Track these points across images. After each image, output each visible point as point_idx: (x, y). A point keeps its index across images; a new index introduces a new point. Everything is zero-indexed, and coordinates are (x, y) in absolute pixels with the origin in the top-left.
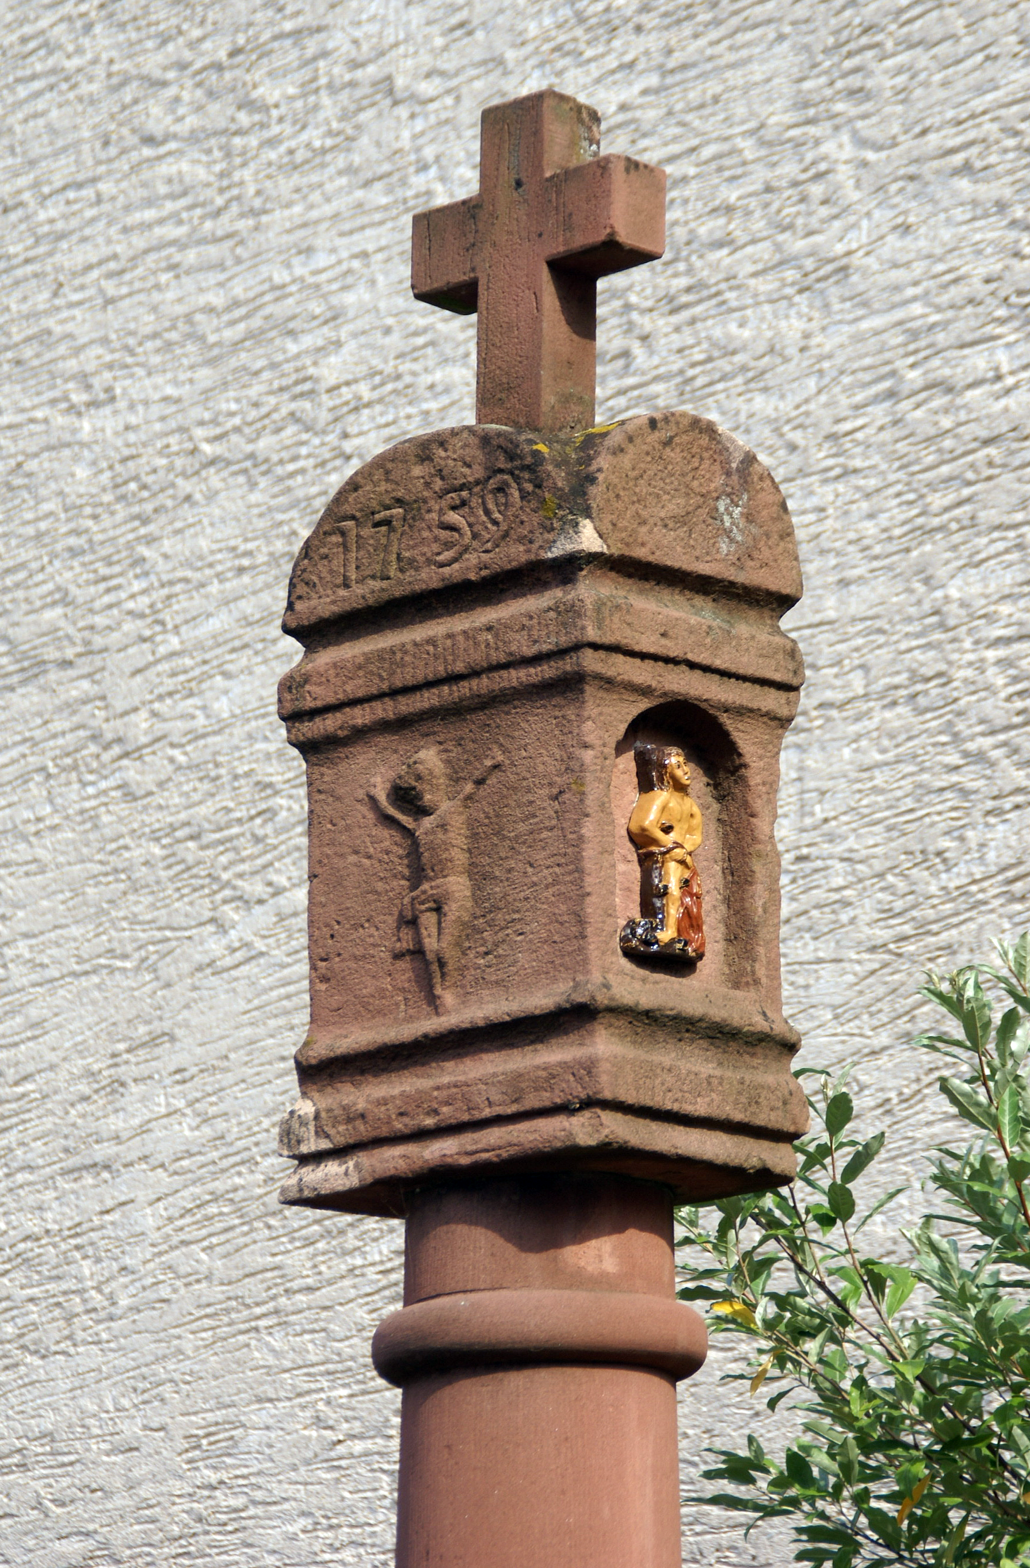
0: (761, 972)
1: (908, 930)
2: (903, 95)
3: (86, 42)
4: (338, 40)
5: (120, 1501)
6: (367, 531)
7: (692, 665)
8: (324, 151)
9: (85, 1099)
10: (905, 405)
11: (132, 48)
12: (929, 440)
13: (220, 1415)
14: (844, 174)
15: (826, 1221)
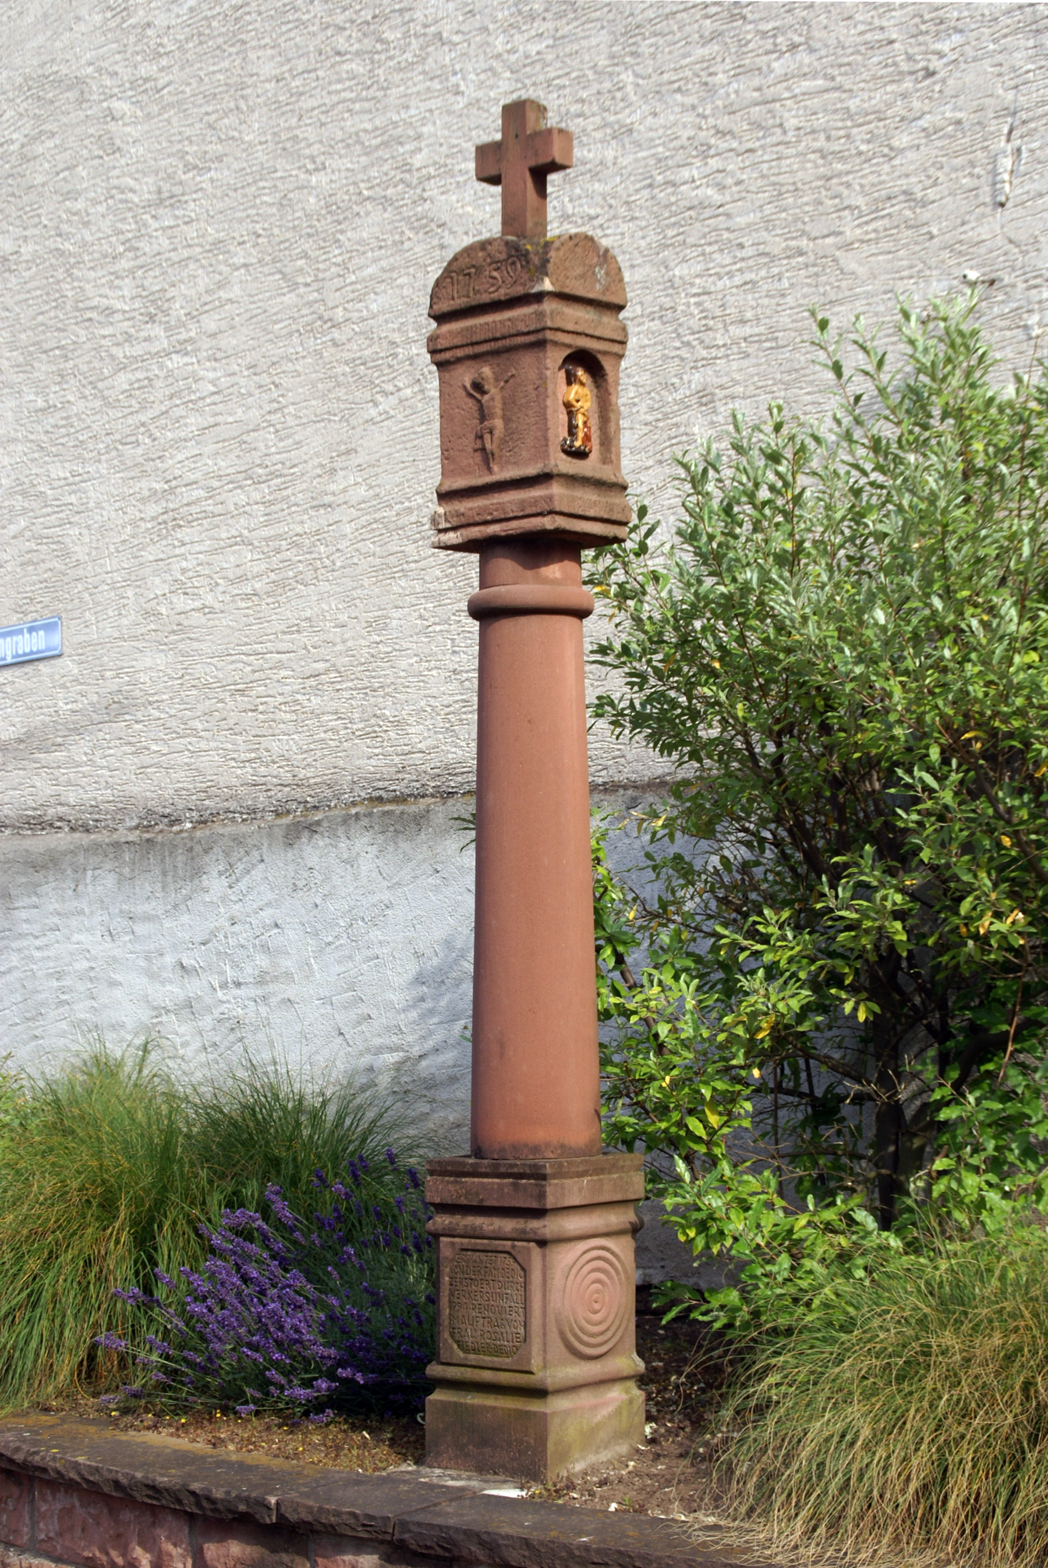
0: (613, 457)
1: (660, 416)
2: (654, 56)
3: (311, 8)
4: (418, 15)
5: (339, 647)
6: (461, 278)
7: (587, 335)
8: (413, 63)
9: (319, 476)
10: (656, 191)
11: (331, 13)
12: (666, 206)
13: (380, 613)
14: (630, 88)
15: (637, 555)
